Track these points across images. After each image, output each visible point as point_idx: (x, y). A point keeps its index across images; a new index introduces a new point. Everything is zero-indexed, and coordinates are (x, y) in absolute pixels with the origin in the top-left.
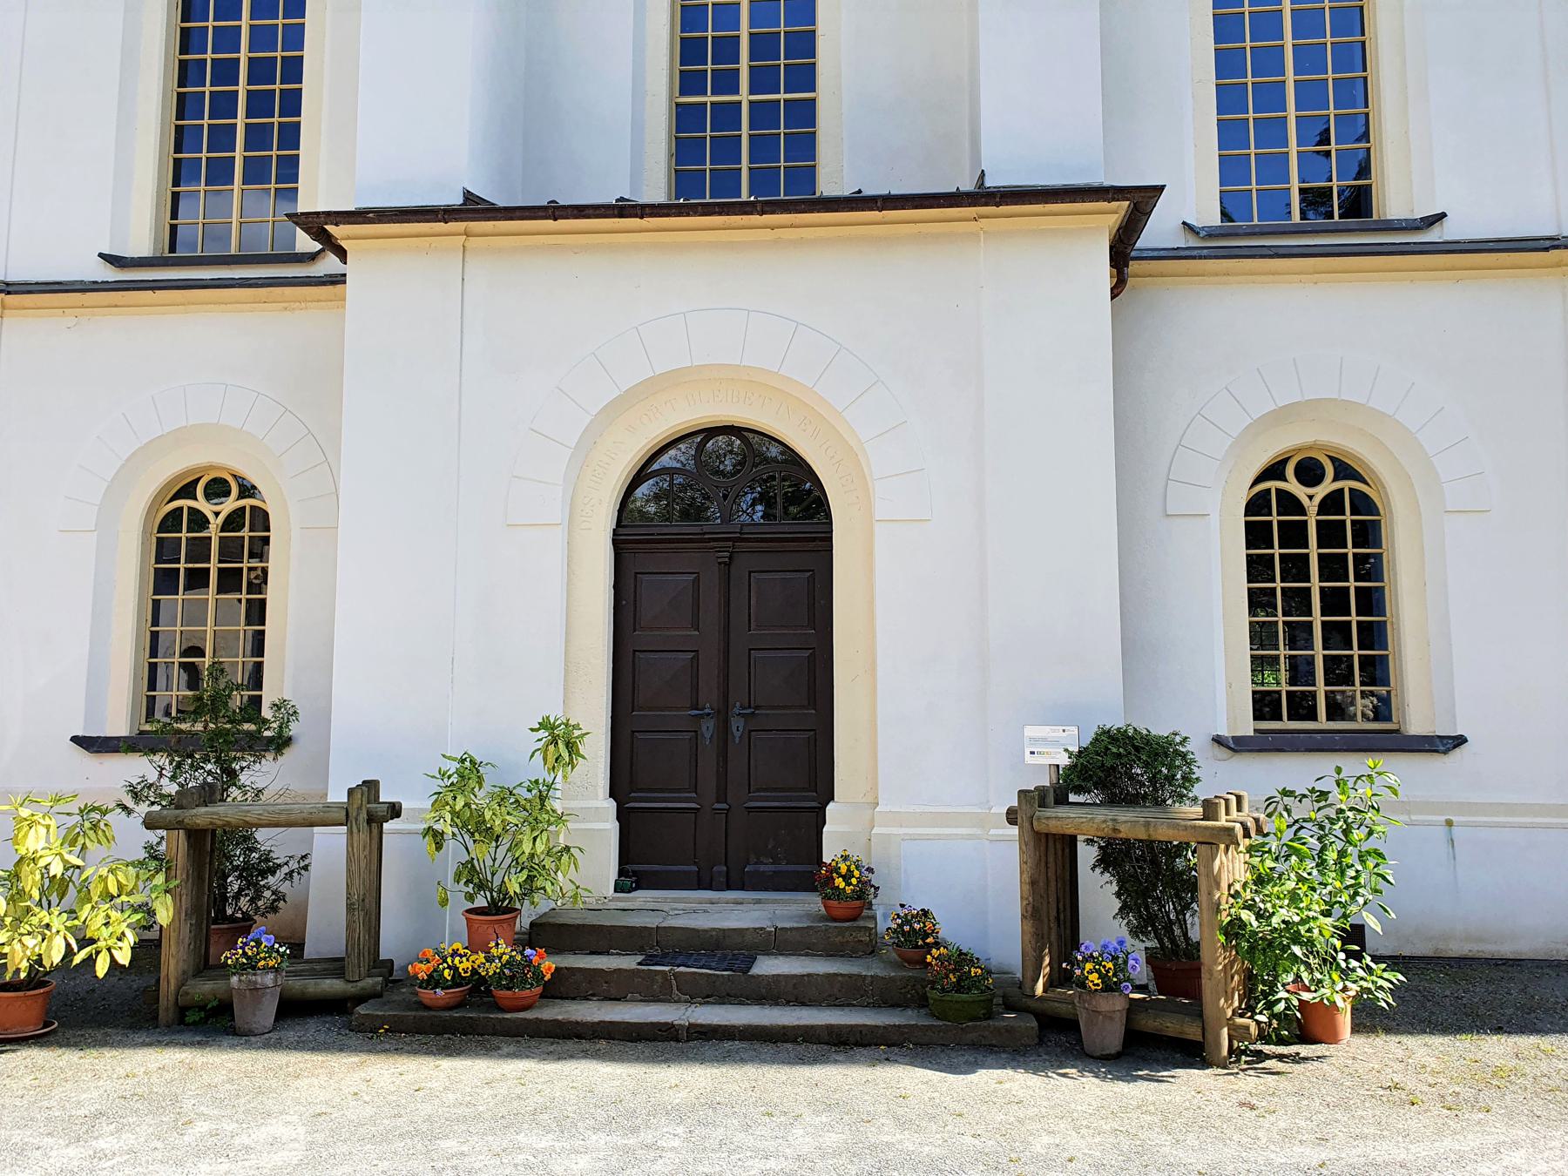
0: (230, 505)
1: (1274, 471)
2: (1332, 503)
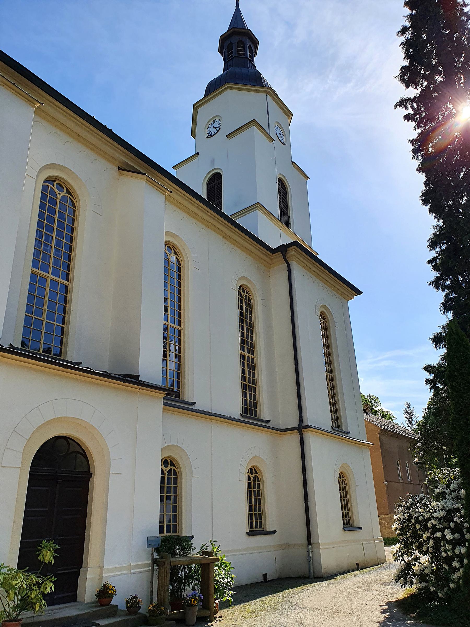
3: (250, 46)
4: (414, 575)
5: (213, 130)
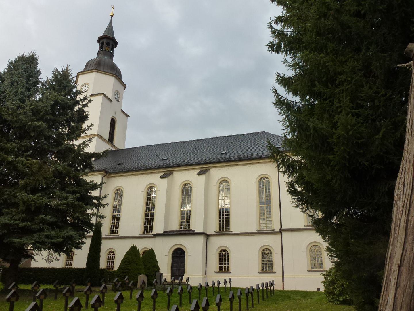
0: (268, 251)
1: (221, 251)
2: (225, 254)
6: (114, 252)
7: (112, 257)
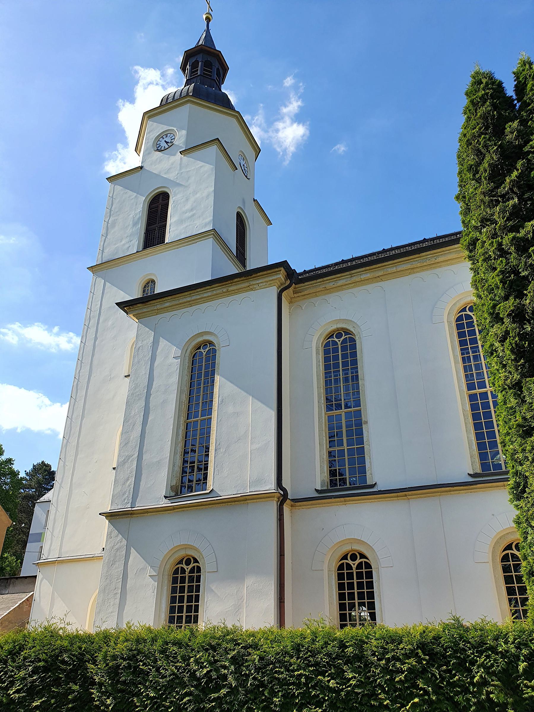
2: (359, 566)
3: (218, 69)
4: (518, 170)
5: (163, 144)
6: (196, 561)
7: (191, 579)
